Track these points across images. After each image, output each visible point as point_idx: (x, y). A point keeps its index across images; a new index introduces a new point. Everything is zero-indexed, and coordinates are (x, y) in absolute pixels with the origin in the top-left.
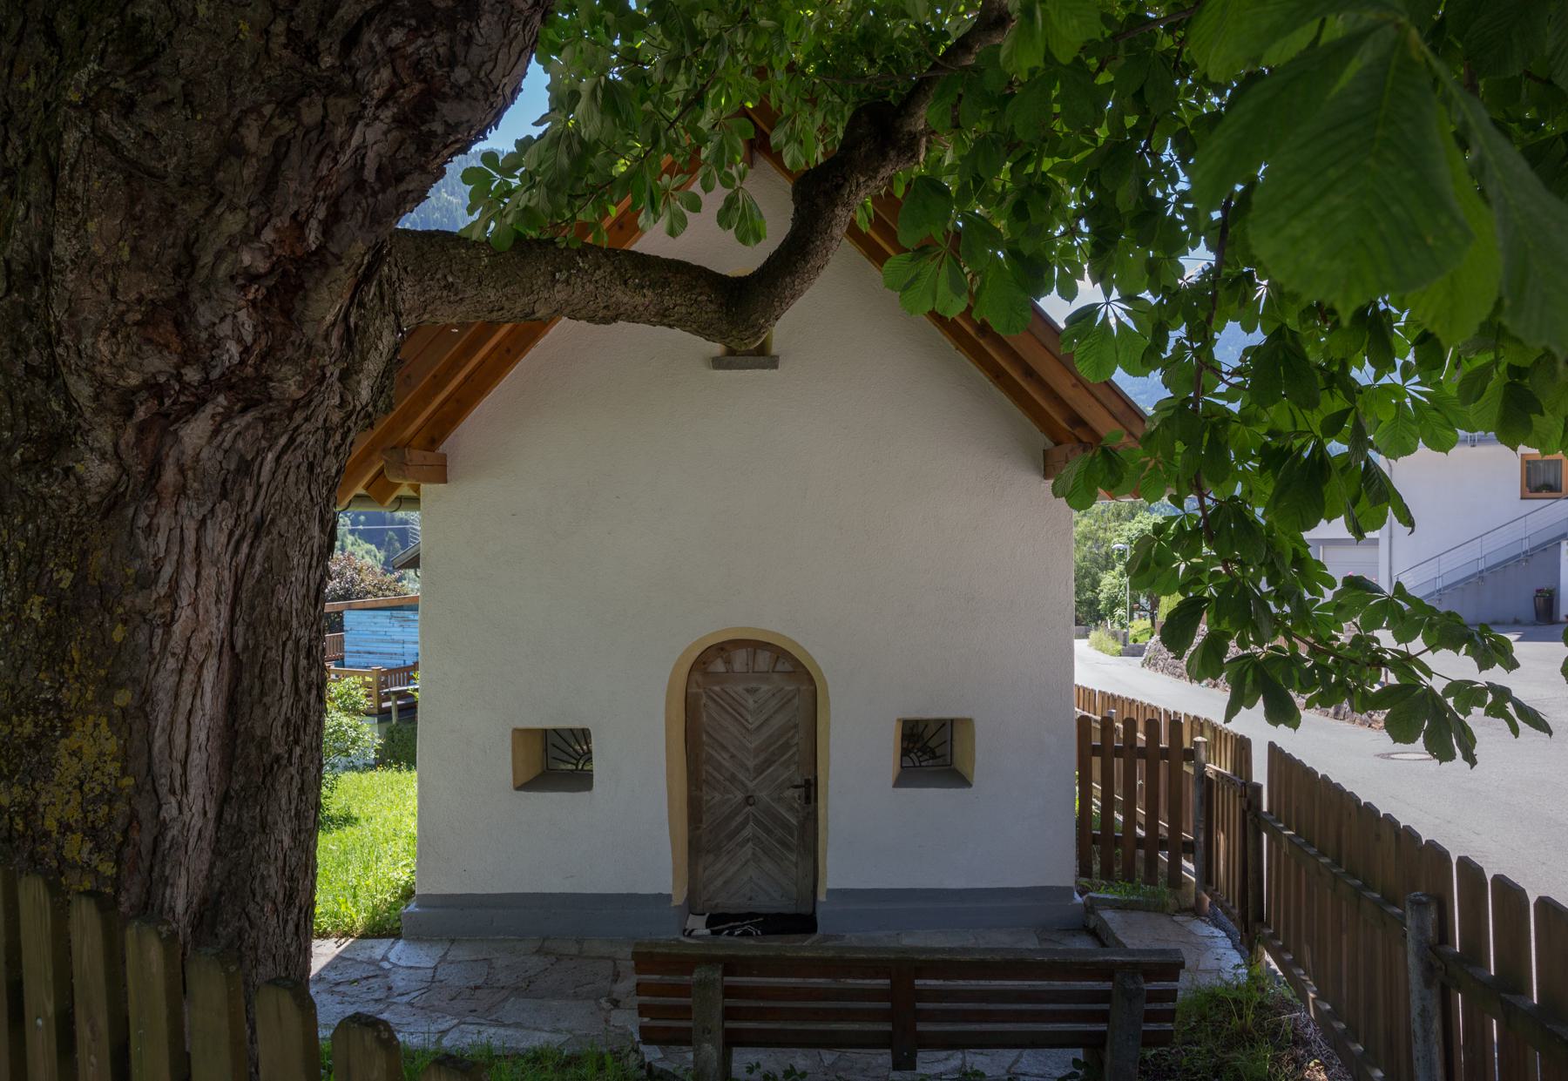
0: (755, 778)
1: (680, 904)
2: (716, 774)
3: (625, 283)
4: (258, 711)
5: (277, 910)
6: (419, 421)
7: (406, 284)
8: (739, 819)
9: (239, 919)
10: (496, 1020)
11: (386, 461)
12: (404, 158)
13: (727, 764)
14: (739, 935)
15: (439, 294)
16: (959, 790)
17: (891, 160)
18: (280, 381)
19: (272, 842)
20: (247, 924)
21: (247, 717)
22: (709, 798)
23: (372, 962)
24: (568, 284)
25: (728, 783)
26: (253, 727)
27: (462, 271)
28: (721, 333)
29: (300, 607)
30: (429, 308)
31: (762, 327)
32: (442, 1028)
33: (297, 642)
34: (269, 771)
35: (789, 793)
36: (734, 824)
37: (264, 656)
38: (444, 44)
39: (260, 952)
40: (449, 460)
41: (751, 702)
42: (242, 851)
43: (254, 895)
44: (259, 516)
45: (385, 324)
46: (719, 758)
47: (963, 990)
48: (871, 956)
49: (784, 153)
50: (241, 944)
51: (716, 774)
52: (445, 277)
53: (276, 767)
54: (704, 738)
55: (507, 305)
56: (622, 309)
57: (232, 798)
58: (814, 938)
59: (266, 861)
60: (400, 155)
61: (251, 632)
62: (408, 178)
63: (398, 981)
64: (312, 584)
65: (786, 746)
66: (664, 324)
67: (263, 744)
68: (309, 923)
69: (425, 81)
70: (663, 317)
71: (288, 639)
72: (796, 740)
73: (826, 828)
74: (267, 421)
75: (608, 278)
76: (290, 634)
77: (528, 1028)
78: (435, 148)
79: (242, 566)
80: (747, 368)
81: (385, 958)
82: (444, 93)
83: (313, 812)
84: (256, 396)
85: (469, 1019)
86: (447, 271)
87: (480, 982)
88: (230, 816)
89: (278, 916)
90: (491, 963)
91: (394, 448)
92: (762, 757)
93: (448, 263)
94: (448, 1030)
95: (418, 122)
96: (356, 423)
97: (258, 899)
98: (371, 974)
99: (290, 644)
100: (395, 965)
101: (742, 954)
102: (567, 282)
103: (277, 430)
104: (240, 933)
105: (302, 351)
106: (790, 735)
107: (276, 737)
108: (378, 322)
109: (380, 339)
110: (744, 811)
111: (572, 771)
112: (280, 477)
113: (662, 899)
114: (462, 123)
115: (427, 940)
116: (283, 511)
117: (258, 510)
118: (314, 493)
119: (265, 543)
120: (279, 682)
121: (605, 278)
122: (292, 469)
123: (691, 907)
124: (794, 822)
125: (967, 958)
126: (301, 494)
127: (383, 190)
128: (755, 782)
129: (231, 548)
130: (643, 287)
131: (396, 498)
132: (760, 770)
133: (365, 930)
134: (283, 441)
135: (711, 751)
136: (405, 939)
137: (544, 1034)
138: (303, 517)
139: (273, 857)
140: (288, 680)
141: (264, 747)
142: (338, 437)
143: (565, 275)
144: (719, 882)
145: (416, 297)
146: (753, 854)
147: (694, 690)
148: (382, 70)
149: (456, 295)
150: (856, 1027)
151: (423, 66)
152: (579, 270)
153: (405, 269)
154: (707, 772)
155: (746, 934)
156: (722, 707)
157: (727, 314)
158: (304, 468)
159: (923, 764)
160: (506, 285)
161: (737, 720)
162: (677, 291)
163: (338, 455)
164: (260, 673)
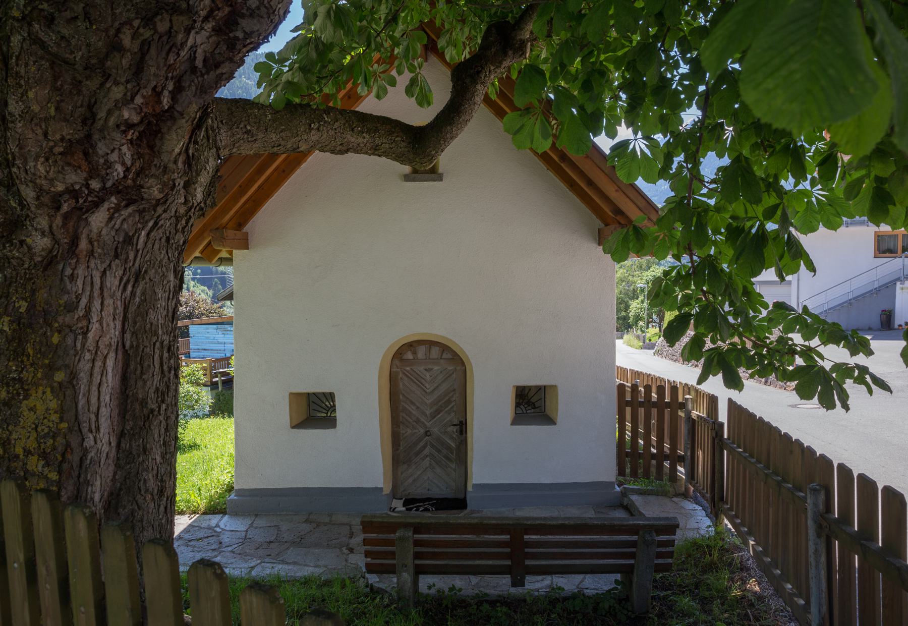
3: (353, 130)
4: (140, 383)
5: (154, 499)
7: (222, 131)
8: (422, 444)
9: (132, 504)
10: (282, 561)
11: (213, 237)
12: (220, 53)
13: (414, 412)
14: (422, 511)
18: (148, 188)
19: (150, 460)
20: (136, 508)
21: (133, 387)
22: (404, 432)
23: (209, 528)
24: (319, 131)
25: (415, 423)
27: (255, 123)
28: (409, 159)
29: (163, 322)
30: (236, 145)
31: (434, 156)
32: (251, 565)
33: (162, 343)
34: (147, 419)
36: (419, 447)
37: (143, 352)
39: (144, 523)
42: (132, 465)
43: (140, 491)
45: (210, 154)
46: (410, 409)
50: (133, 519)
52: (245, 126)
53: (151, 416)
55: (283, 143)
57: (126, 434)
58: (466, 512)
60: (217, 51)
61: (134, 338)
62: (222, 66)
63: (225, 539)
64: (170, 309)
65: (449, 402)
66: (376, 155)
67: (143, 403)
69: (231, 6)
70: (375, 151)
71: (156, 341)
72: (454, 399)
73: (472, 449)
74: (141, 212)
75: (342, 127)
76: (158, 338)
77: (300, 565)
79: (128, 299)
80: (425, 181)
82: (243, 13)
85: (267, 560)
86: (246, 123)
87: (273, 539)
91: (217, 229)
94: (255, 566)
95: (227, 31)
97: (143, 492)
99: (158, 344)
100: (223, 530)
101: (424, 521)
102: (318, 129)
103: (147, 218)
105: (161, 170)
106: (450, 395)
107: (151, 398)
111: (324, 417)
112: (150, 245)
114: (254, 32)
115: (242, 515)
116: (152, 266)
117: (137, 265)
118: (170, 255)
119: (142, 284)
120: (152, 366)
122: (157, 241)
123: (394, 495)
125: (554, 523)
127: (208, 73)
128: (430, 423)
129: (121, 287)
130: (363, 133)
131: (219, 258)
132: (433, 416)
134: (151, 224)
135: (407, 406)
137: (311, 568)
138: (164, 269)
139: (150, 468)
142: (183, 222)
144: (410, 480)
146: (430, 464)
147: (395, 369)
150: (490, 562)
152: (325, 122)
153: (222, 121)
154: (403, 417)
155: (426, 510)
157: (413, 148)
158: (163, 240)
159: (528, 412)
161: (419, 386)
162: (383, 135)
164: (141, 361)
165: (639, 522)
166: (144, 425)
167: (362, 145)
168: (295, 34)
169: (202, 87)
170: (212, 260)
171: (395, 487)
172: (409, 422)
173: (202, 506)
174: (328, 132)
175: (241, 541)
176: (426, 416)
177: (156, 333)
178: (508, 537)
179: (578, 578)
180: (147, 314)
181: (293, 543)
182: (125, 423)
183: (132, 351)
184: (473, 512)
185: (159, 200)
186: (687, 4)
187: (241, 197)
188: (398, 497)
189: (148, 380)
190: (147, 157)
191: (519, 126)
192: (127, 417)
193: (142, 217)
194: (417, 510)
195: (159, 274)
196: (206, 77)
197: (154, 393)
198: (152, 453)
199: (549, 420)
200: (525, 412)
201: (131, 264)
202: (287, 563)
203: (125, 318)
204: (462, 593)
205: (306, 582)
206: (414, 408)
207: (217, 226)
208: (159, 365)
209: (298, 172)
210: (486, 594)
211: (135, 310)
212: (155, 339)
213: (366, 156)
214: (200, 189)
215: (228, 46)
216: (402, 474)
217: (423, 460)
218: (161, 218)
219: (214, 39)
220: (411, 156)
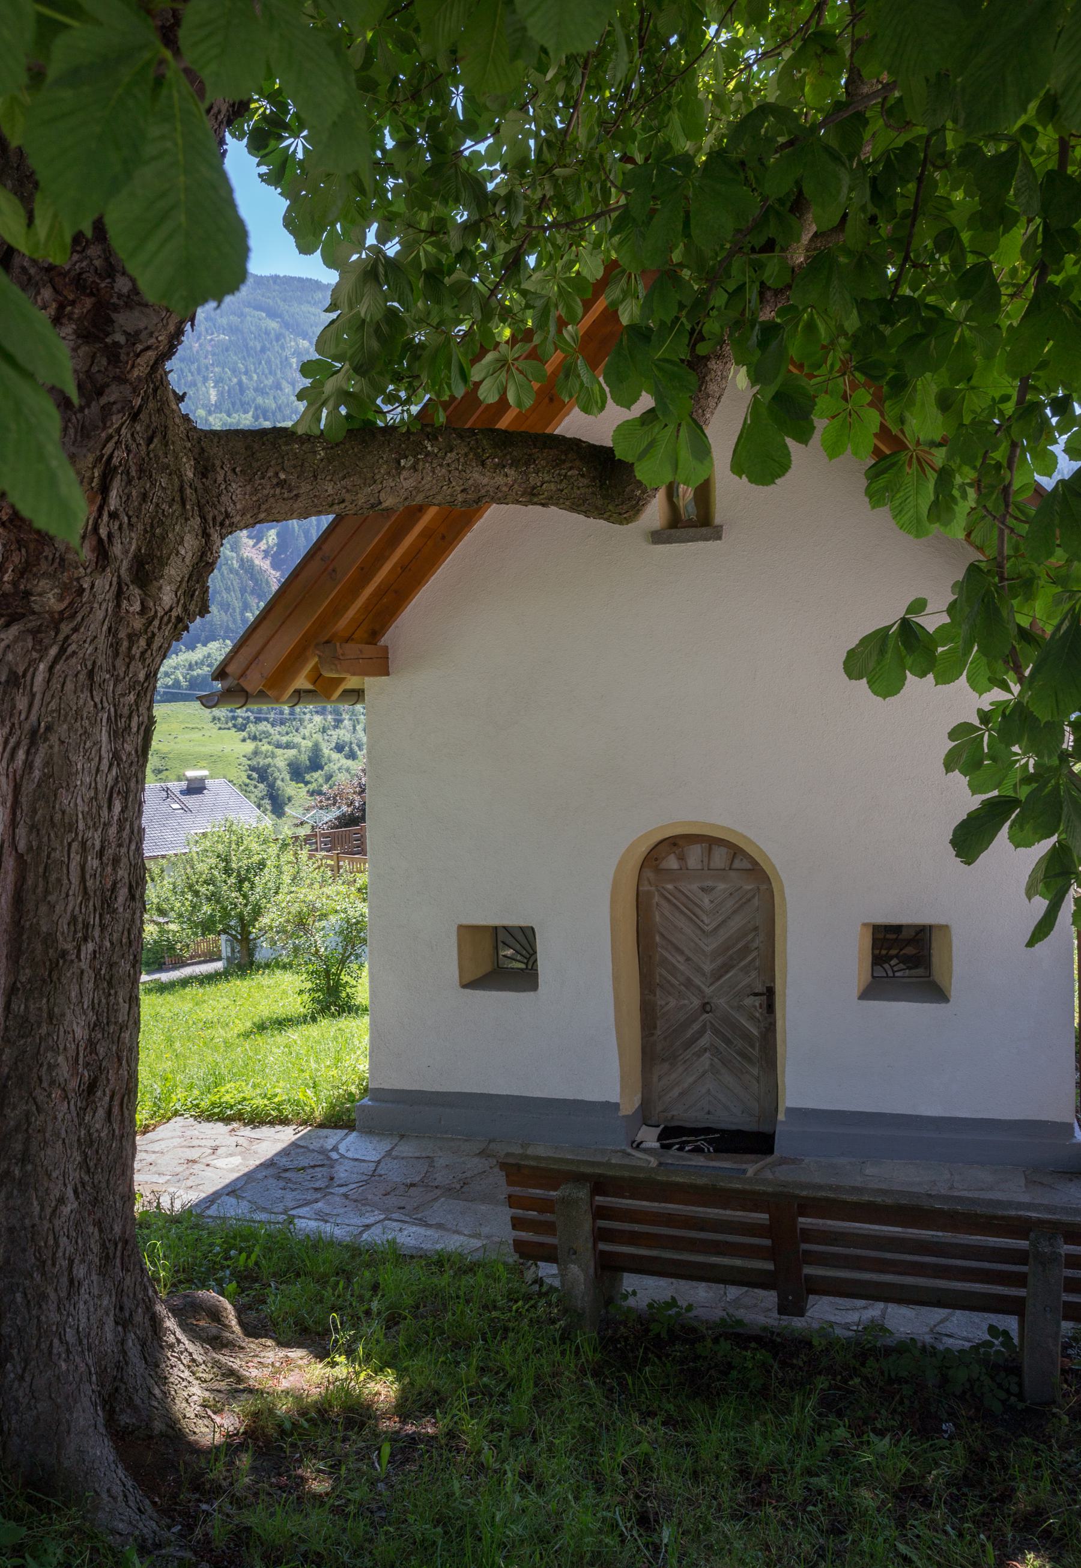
0: (711, 984)
1: (630, 1113)
2: (670, 978)
3: (483, 464)
4: (43, 909)
5: (67, 1097)
6: (351, 613)
7: (234, 486)
8: (696, 1027)
9: (27, 1103)
10: (420, 1220)
11: (320, 657)
12: (99, 371)
13: (682, 968)
14: (689, 1151)
15: (272, 492)
16: (934, 1006)
17: (768, 301)
18: (40, 595)
19: (62, 1033)
20: (34, 1108)
21: (32, 913)
22: (663, 1003)
23: (323, 1151)
24: (416, 470)
25: (682, 987)
26: (38, 924)
27: (295, 467)
28: (597, 508)
29: (86, 809)
30: (264, 507)
31: (639, 499)
32: (367, 1222)
33: (83, 844)
34: (54, 966)
35: (749, 1001)
36: (690, 1033)
37: (48, 857)
38: (100, 257)
39: (47, 1135)
40: (390, 652)
41: (706, 901)
42: (29, 1040)
43: (41, 1081)
44: (36, 724)
45: (187, 529)
46: (674, 961)
47: (857, 1235)
48: (747, 1187)
49: (620, 313)
50: (29, 1126)
51: (670, 978)
52: (277, 474)
53: (61, 962)
54: (657, 938)
55: (348, 497)
56: (483, 492)
57: (18, 989)
58: (769, 1159)
59: (53, 1050)
60: (95, 369)
61: (34, 834)
62: (107, 391)
63: (342, 1173)
64: (99, 787)
65: (746, 950)
66: (535, 504)
67: (49, 940)
68: (126, 1113)
69: (92, 294)
70: (532, 496)
71: (73, 841)
72: (755, 945)
73: (784, 1042)
74: (35, 632)
75: (462, 460)
76: (77, 834)
77: (448, 1230)
78: (123, 357)
79: (19, 772)
80: (689, 541)
81: (335, 1149)
82: (114, 304)
83: (127, 1005)
84: (20, 610)
85: (395, 1216)
86: (278, 468)
87: (417, 1179)
88: (18, 1007)
89: (69, 1103)
90: (433, 1161)
91: (327, 642)
92: (719, 961)
93: (280, 461)
94: (373, 1225)
95: (102, 335)
96: (160, 628)
97: (45, 1085)
98: (319, 1163)
99: (75, 845)
100: (342, 1156)
101: (610, 1173)
102: (414, 468)
103: (46, 641)
104: (27, 1115)
105: (56, 565)
106: (750, 937)
107: (63, 933)
108: (177, 528)
109: (181, 542)
110: (701, 1019)
111: (522, 970)
112: (56, 685)
113: (610, 1107)
114: (141, 331)
115: (378, 1134)
116: (62, 718)
117: (33, 717)
118: (97, 700)
119: (43, 749)
120: (66, 881)
121: (458, 460)
122: (69, 678)
123: (645, 1115)
124: (755, 1032)
125: (854, 1198)
126: (81, 702)
127: (88, 405)
128: (712, 988)
129: (6, 755)
130: (504, 467)
131: (295, 691)
132: (718, 975)
133: (326, 1118)
134: (53, 651)
135: (667, 955)
136: (361, 1132)
137: (462, 1238)
138: (86, 723)
139: (61, 1047)
140: (75, 879)
141: (49, 943)
142: (142, 643)
143: (411, 460)
144: (676, 1092)
145: (247, 497)
146: (711, 1065)
147: (645, 888)
148: (42, 291)
149: (290, 491)
150: (738, 1262)
151: (85, 280)
152: (428, 454)
153: (234, 470)
154: (661, 975)
155: (698, 1150)
156: (674, 905)
157: (601, 487)
158: (82, 677)
159: (897, 974)
160: (344, 477)
161: (691, 920)
162: (544, 467)
163: (145, 660)
164: (45, 873)
165: (1029, 1214)
166: (50, 975)
167: (505, 489)
168: (333, 316)
169: (83, 427)
170: (331, 695)
171: (646, 1104)
172: (672, 986)
173: (319, 1114)
174: (434, 472)
175: (365, 1178)
176: (704, 974)
177: (72, 827)
178: (767, 1216)
179: (938, 1314)
180: (55, 795)
181: (449, 1192)
182: (18, 972)
183: (30, 856)
184: (783, 1161)
185: (61, 613)
187: (363, 587)
188: (653, 1123)
189: (57, 902)
190: (32, 546)
191: (646, 443)
192: (22, 962)
193: (38, 642)
194: (681, 1149)
195: (77, 730)
196: (86, 411)
197: (69, 924)
198: (66, 1023)
199: (937, 993)
200: (890, 974)
201: (23, 717)
202: (427, 1225)
203: (16, 803)
204: (691, 1314)
205: (439, 1262)
206: (681, 959)
207: (326, 639)
208: (78, 879)
209: (469, 537)
210: (740, 1322)
211: (35, 791)
212: (70, 837)
213: (518, 506)
214: (168, 588)
215: (108, 359)
216: (659, 1080)
217: (699, 1056)
218: (70, 641)
219: (84, 349)
220: (599, 502)
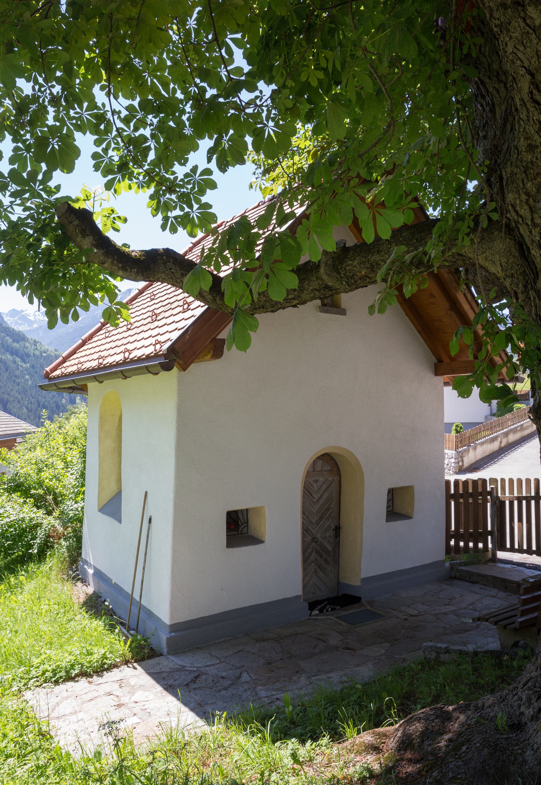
65: (328, 509)
132: (318, 522)
186: (336, 93)
